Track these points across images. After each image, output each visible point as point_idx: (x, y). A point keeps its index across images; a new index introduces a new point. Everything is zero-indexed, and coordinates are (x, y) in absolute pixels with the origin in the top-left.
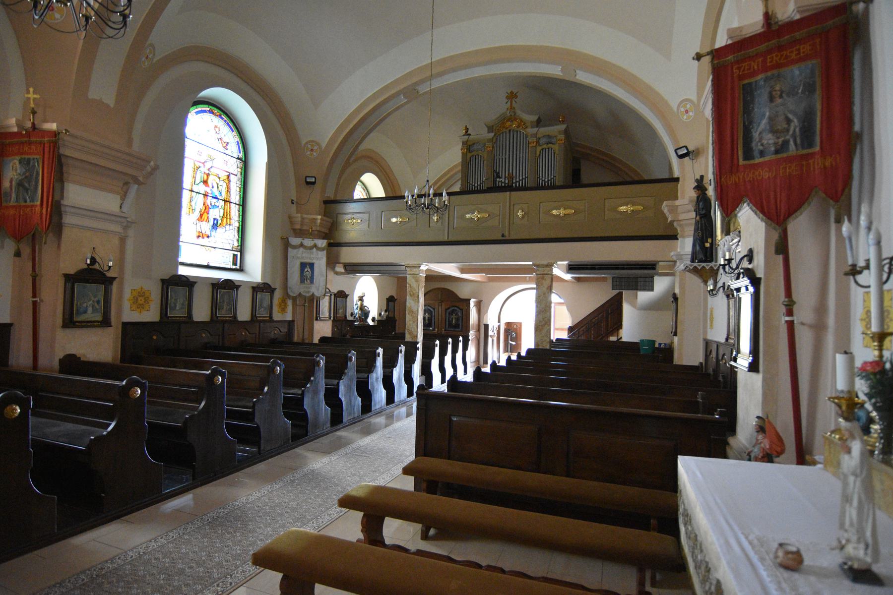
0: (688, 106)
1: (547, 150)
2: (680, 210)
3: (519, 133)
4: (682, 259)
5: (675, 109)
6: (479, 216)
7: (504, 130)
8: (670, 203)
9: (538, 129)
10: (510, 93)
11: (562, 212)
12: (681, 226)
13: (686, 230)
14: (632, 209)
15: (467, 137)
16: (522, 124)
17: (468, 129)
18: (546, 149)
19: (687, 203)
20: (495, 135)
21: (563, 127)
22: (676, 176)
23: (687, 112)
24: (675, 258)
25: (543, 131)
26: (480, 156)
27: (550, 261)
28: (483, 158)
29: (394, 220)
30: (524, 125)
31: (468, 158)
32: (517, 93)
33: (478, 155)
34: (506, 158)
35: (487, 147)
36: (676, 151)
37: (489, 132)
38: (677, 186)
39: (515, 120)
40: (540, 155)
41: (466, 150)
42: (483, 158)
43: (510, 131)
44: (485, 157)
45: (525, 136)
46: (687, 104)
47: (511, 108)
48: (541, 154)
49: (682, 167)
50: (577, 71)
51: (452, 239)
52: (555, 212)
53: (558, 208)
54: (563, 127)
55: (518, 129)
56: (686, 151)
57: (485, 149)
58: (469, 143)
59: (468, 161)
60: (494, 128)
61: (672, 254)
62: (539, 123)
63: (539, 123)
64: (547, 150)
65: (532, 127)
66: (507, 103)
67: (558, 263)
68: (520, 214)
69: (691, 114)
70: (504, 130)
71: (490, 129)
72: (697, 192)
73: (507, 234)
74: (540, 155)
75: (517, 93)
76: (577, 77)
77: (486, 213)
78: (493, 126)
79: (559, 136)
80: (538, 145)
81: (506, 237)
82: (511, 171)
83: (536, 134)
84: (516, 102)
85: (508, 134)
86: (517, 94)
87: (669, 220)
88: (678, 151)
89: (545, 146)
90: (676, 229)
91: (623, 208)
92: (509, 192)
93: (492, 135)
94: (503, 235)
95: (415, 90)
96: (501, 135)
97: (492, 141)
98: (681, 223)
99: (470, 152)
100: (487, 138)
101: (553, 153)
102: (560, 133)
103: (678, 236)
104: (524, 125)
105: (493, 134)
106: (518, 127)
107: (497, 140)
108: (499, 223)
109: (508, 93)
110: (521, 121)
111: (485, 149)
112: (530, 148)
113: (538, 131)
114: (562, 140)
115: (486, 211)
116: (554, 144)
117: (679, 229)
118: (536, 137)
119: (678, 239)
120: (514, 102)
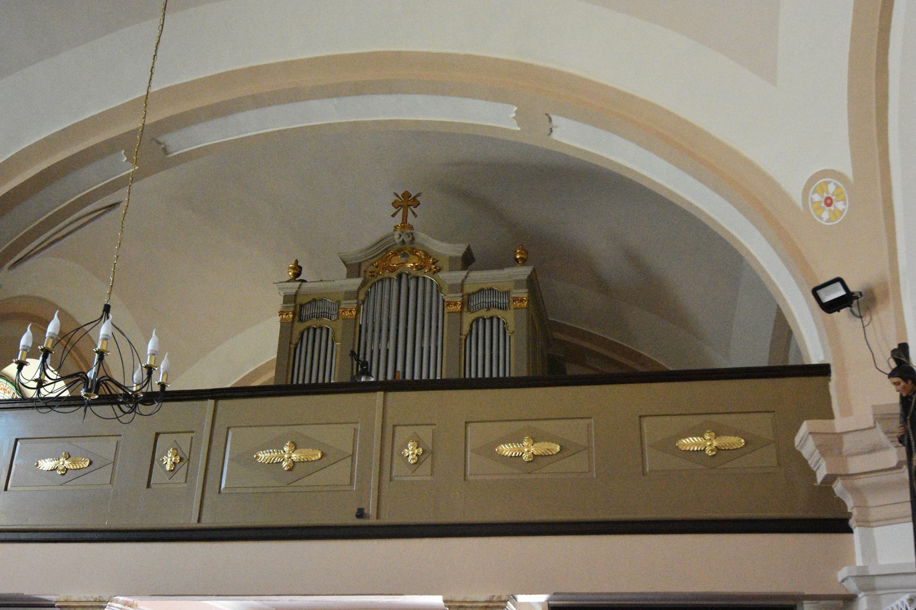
0: (831, 188)
1: (488, 323)
2: (848, 443)
3: (421, 281)
4: (874, 589)
5: (797, 198)
6: (295, 456)
7: (387, 274)
8: (819, 425)
9: (464, 273)
10: (403, 195)
11: (528, 449)
12: (855, 491)
13: (871, 501)
14: (715, 443)
15: (298, 284)
16: (430, 262)
17: (301, 268)
18: (484, 320)
19: (870, 423)
20: (363, 285)
21: (523, 272)
22: (814, 361)
23: (829, 202)
24: (852, 587)
25: (479, 278)
26: (324, 331)
27: (497, 594)
28: (334, 333)
29: (46, 464)
30: (433, 264)
31: (296, 335)
32: (419, 195)
33: (321, 328)
34: (387, 351)
35: (345, 310)
36: (815, 291)
37: (349, 276)
38: (827, 387)
39: (413, 252)
40: (471, 331)
41: (291, 316)
42: (334, 333)
43: (400, 277)
44: (339, 333)
45: (435, 287)
46: (827, 183)
47: (403, 227)
48: (474, 331)
49: (832, 337)
50: (554, 117)
51: (208, 521)
52: (506, 450)
53: (516, 439)
54: (523, 272)
55: (420, 274)
56: (842, 293)
57: (338, 314)
58: (300, 300)
59: (294, 342)
60: (363, 268)
61: (842, 573)
62: (467, 261)
63: (467, 261)
64: (488, 323)
65: (451, 269)
66: (393, 216)
67: (521, 598)
68: (411, 452)
69: (840, 205)
70: (387, 274)
71: (353, 270)
72: (903, 384)
73: (371, 510)
74: (471, 331)
75: (419, 195)
76: (555, 136)
77: (314, 447)
78: (360, 264)
79: (514, 291)
80: (465, 309)
81: (368, 516)
82: (399, 368)
83: (462, 285)
84: (414, 213)
85: (395, 285)
86: (418, 199)
87: (820, 475)
88: (821, 293)
89: (483, 313)
90: (841, 503)
91: (690, 443)
92: (382, 393)
93: (357, 282)
94: (361, 514)
95: (159, 143)
96: (380, 285)
97: (357, 298)
98: (860, 482)
99: (301, 320)
100: (345, 289)
101: (501, 329)
102: (518, 284)
103: (852, 523)
104: (433, 264)
105: (359, 281)
106: (420, 268)
107: (367, 295)
108: (352, 478)
109: (397, 196)
110: (427, 255)
111: (338, 314)
112: (446, 316)
113: (466, 277)
114: (522, 300)
115: (310, 443)
116: (505, 308)
117: (850, 503)
118: (462, 291)
119: (850, 531)
120: (410, 214)
